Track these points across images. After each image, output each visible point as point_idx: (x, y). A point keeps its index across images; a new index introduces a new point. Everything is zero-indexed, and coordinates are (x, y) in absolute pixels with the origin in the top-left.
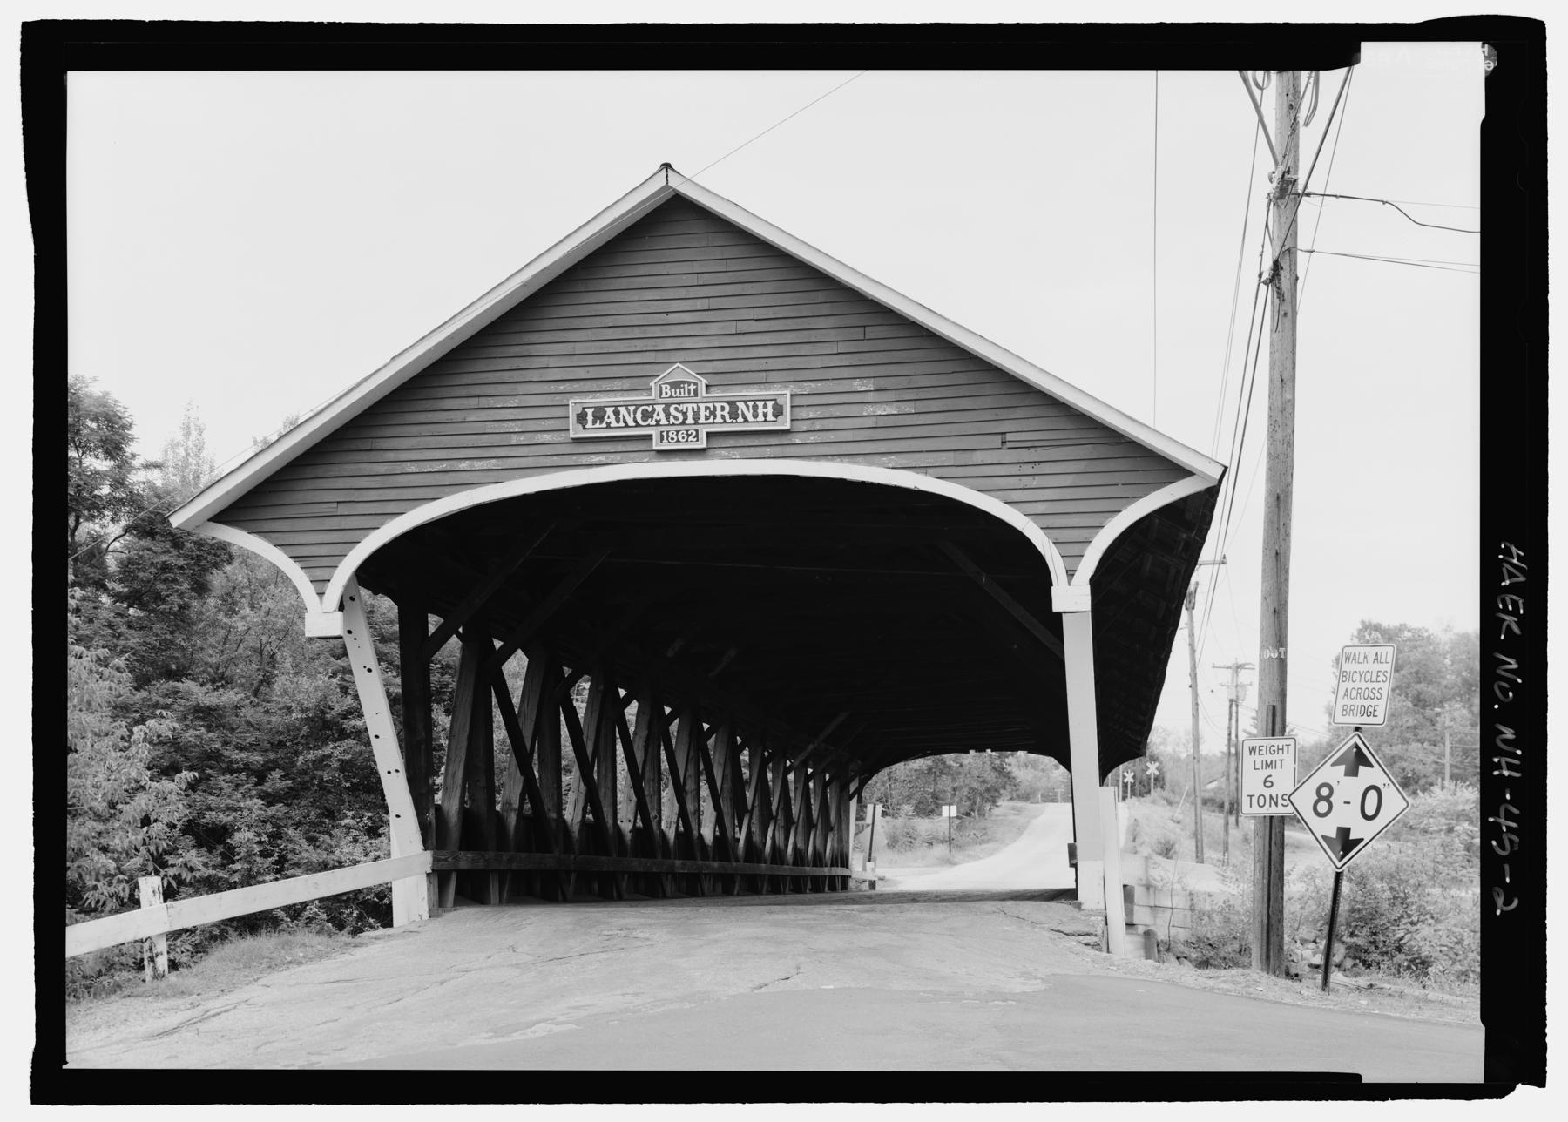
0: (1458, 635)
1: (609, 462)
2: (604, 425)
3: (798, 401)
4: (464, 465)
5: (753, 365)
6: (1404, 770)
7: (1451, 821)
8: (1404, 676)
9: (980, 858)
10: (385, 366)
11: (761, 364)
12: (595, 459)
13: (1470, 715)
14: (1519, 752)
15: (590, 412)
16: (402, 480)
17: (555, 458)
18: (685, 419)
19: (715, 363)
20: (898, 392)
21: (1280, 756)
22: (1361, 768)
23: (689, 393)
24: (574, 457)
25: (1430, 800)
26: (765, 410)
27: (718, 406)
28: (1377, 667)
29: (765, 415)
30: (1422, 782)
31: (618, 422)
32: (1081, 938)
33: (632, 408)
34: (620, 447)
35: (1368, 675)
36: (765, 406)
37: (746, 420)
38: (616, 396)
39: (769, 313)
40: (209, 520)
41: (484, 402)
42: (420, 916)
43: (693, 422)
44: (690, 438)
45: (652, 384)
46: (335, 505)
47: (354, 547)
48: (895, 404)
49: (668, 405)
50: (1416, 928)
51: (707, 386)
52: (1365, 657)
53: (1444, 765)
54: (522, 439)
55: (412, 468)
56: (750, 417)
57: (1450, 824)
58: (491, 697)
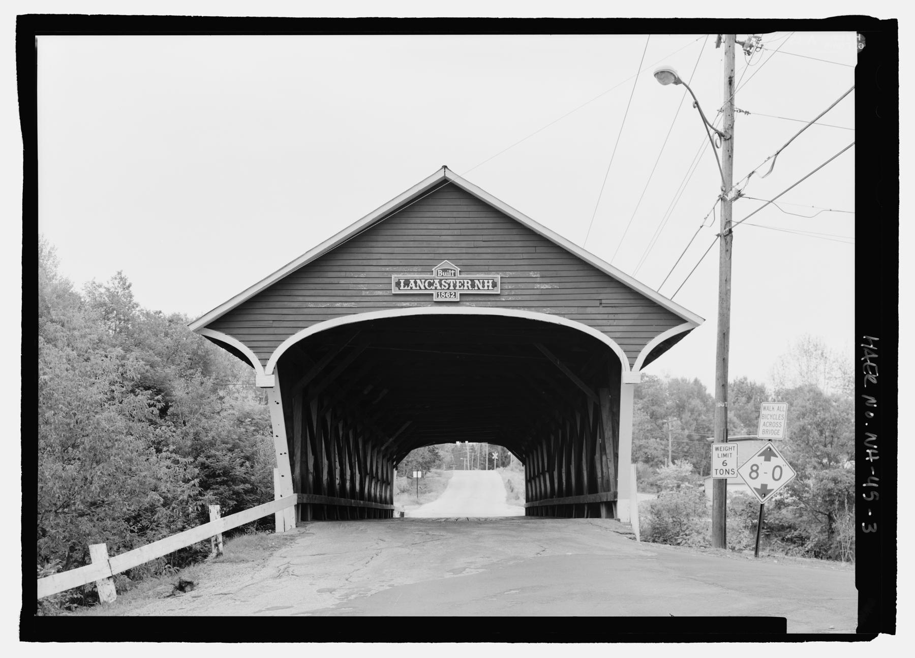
0: (673, 379)
1: (411, 305)
2: (409, 288)
3: (505, 280)
4: (338, 305)
5: (482, 262)
6: (646, 453)
7: (679, 482)
8: (645, 402)
9: (432, 501)
10: (302, 255)
11: (486, 262)
12: (404, 304)
13: (681, 424)
14: (875, 447)
15: (402, 281)
16: (306, 311)
17: (384, 303)
18: (449, 286)
19: (463, 260)
20: (551, 278)
21: (730, 451)
22: (772, 457)
23: (451, 275)
24: (394, 303)
25: (668, 471)
26: (488, 284)
27: (466, 281)
28: (779, 413)
29: (488, 286)
30: (656, 460)
31: (416, 287)
32: (627, 535)
33: (423, 281)
34: (416, 299)
35: (775, 417)
36: (488, 282)
37: (479, 289)
38: (414, 274)
39: (490, 238)
40: (205, 327)
41: (348, 274)
42: (291, 526)
43: (453, 288)
44: (452, 296)
45: (433, 269)
46: (272, 322)
47: (281, 343)
48: (549, 284)
49: (441, 280)
50: (688, 537)
51: (460, 271)
52: (773, 408)
53: (668, 451)
54: (367, 293)
55: (311, 305)
56: (481, 287)
57: (678, 483)
58: (580, 431)
